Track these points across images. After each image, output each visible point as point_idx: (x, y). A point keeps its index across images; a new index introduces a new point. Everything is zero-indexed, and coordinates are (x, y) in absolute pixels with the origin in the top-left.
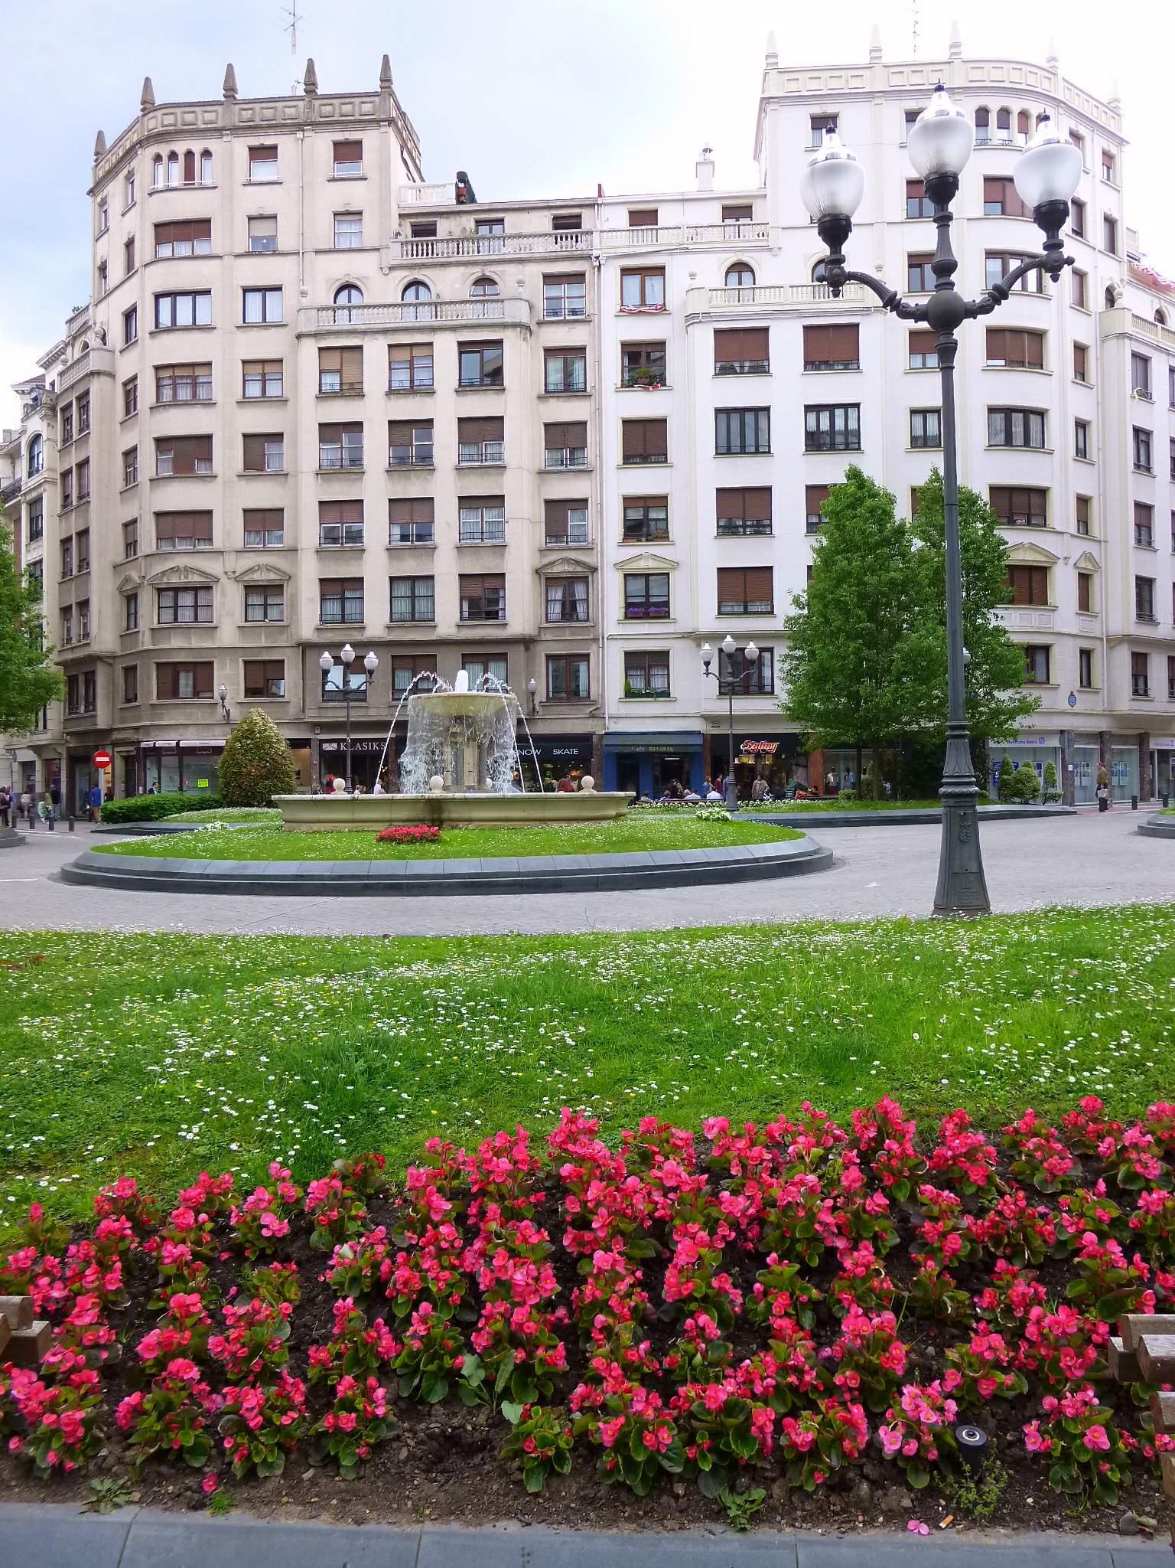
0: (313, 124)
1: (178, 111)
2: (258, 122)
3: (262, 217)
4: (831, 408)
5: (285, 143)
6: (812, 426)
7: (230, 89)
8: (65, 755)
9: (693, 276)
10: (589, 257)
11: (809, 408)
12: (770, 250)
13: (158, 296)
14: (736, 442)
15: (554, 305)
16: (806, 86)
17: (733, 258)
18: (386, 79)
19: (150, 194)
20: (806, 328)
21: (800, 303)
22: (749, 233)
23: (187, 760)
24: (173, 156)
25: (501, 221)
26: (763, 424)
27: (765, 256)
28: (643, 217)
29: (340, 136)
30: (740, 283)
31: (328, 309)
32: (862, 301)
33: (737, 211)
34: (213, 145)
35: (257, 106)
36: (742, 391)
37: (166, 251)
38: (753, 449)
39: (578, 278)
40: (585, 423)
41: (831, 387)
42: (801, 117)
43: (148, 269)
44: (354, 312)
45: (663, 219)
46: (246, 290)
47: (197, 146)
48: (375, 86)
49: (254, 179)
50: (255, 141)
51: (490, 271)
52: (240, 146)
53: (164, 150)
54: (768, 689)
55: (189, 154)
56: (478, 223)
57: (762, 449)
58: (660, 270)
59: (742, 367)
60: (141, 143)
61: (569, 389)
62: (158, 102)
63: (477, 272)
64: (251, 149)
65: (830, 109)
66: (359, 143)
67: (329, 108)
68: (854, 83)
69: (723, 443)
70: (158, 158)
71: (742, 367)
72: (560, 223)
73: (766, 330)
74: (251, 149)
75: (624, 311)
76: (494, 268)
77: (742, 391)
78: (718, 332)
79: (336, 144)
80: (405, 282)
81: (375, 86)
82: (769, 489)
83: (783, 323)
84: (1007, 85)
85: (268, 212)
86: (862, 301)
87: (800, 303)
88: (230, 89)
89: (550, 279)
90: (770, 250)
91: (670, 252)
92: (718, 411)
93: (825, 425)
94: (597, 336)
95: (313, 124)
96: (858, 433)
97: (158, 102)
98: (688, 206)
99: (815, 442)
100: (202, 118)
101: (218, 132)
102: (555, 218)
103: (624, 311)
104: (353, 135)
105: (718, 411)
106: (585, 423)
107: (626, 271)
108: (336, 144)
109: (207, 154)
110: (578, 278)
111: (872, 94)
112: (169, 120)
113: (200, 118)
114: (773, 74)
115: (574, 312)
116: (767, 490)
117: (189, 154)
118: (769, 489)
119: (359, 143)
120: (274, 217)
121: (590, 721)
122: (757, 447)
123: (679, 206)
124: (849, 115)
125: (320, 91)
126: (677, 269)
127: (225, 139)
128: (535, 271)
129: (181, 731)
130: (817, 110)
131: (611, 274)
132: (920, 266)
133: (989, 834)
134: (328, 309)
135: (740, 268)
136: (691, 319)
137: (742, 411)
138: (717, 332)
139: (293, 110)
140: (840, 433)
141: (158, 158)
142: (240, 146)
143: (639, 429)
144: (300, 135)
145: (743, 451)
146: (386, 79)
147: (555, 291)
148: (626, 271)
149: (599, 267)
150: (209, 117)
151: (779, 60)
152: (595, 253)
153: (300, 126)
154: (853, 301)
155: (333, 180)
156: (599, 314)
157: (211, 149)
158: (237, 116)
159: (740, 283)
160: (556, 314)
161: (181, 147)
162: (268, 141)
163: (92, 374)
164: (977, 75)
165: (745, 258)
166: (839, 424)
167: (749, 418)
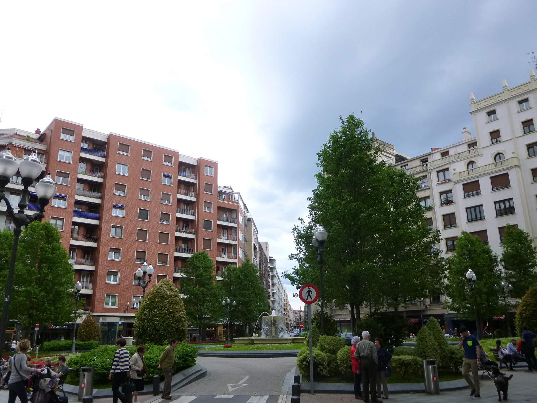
4: (504, 201)
6: (498, 208)
9: (454, 170)
11: (495, 203)
12: (479, 155)
14: (474, 217)
16: (483, 104)
17: (468, 161)
20: (491, 178)
21: (492, 169)
23: (342, 324)
25: (407, 165)
27: (478, 158)
28: (445, 154)
30: (473, 167)
32: (508, 165)
33: (472, 145)
36: (473, 201)
38: (479, 219)
39: (425, 177)
40: (432, 218)
41: (503, 194)
42: (483, 115)
56: (402, 167)
57: (482, 218)
58: (447, 169)
59: (473, 194)
61: (449, 202)
65: (492, 109)
68: (499, 99)
69: (470, 218)
71: (473, 194)
73: (507, 173)
75: (438, 184)
77: (473, 201)
78: (463, 185)
82: (486, 230)
83: (481, 178)
86: (508, 165)
87: (492, 169)
90: (479, 155)
91: (449, 164)
92: (467, 209)
93: (507, 206)
96: (513, 208)
99: (500, 213)
102: (421, 160)
103: (438, 184)
105: (467, 209)
106: (432, 218)
107: (438, 172)
110: (425, 177)
111: (505, 100)
114: (473, 105)
115: (426, 186)
116: (485, 231)
118: (486, 230)
121: (443, 310)
122: (481, 217)
124: (500, 110)
126: (451, 167)
129: (340, 316)
130: (488, 110)
131: (434, 175)
132: (532, 147)
133: (440, 388)
135: (471, 163)
136: (456, 183)
137: (474, 207)
138: (463, 185)
140: (508, 208)
145: (477, 219)
149: (430, 173)
152: (428, 169)
154: (476, 174)
156: (432, 186)
159: (473, 167)
164: (513, 93)
165: (472, 160)
166: (507, 206)
167: (477, 209)
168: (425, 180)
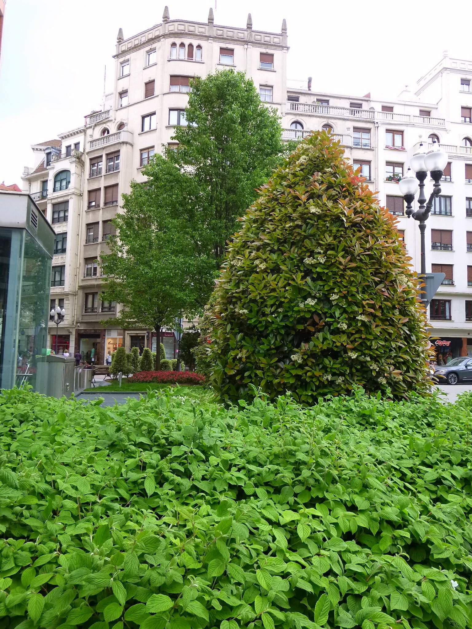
0: (252, 42)
1: (187, 24)
2: (225, 37)
3: (266, 86)
5: (238, 49)
7: (211, 20)
8: (74, 333)
10: (374, 122)
13: (143, 118)
15: (357, 141)
16: (459, 66)
18: (284, 29)
19: (169, 61)
22: (434, 122)
24: (182, 45)
26: (448, 203)
29: (264, 51)
31: (294, 130)
34: (203, 43)
35: (225, 30)
37: (176, 89)
39: (368, 130)
43: (165, 96)
44: (297, 133)
45: (395, 110)
46: (171, 110)
47: (195, 43)
48: (279, 31)
49: (221, 62)
50: (224, 45)
51: (331, 122)
52: (217, 46)
53: (178, 41)
54: (448, 318)
55: (191, 46)
56: (318, 100)
58: (401, 132)
60: (164, 36)
62: (172, 18)
63: (325, 121)
64: (221, 49)
66: (272, 55)
67: (259, 37)
70: (174, 45)
72: (352, 105)
74: (221, 49)
76: (333, 121)
79: (261, 54)
80: (293, 121)
81: (279, 31)
84: (467, 70)
85: (269, 84)
88: (211, 20)
89: (356, 129)
94: (376, 156)
95: (252, 42)
97: (172, 18)
98: (407, 107)
100: (198, 30)
101: (208, 38)
104: (270, 52)
108: (261, 54)
109: (199, 47)
110: (368, 130)
112: (182, 27)
113: (197, 29)
116: (450, 232)
117: (191, 46)
119: (272, 55)
120: (272, 87)
123: (403, 107)
125: (253, 29)
127: (210, 41)
128: (351, 125)
130: (464, 77)
134: (294, 130)
139: (242, 35)
141: (174, 45)
142: (217, 46)
143: (391, 199)
144: (246, 46)
146: (284, 29)
147: (358, 135)
148: (388, 131)
150: (201, 30)
151: (253, 26)
153: (246, 42)
155: (261, 70)
157: (202, 45)
158: (215, 32)
160: (356, 145)
161: (187, 41)
162: (230, 46)
163: (123, 143)
168: (365, 136)
